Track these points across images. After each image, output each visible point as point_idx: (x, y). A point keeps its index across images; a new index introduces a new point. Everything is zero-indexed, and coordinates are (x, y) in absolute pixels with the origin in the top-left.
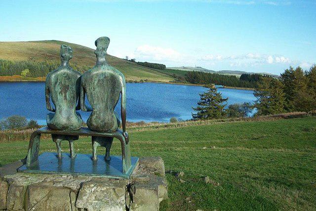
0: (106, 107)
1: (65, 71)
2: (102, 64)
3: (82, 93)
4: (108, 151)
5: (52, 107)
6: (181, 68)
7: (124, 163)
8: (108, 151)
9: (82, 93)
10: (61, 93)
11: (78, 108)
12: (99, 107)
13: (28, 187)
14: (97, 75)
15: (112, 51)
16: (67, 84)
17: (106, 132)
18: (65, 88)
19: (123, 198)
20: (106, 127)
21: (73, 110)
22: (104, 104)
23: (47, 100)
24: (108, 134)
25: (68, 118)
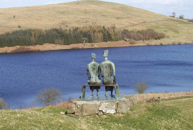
0: (109, 75)
1: (94, 62)
2: (106, 60)
3: (100, 71)
4: (112, 93)
5: (89, 76)
6: (57, 4)
7: (116, 96)
8: (112, 93)
9: (100, 71)
10: (92, 71)
11: (99, 76)
12: (106, 75)
13: (82, 105)
14: (104, 64)
15: (161, 98)
16: (94, 67)
17: (109, 84)
18: (94, 69)
19: (114, 106)
20: (109, 82)
21: (97, 77)
22: (108, 74)
23: (88, 73)
24: (109, 85)
25: (95, 80)
